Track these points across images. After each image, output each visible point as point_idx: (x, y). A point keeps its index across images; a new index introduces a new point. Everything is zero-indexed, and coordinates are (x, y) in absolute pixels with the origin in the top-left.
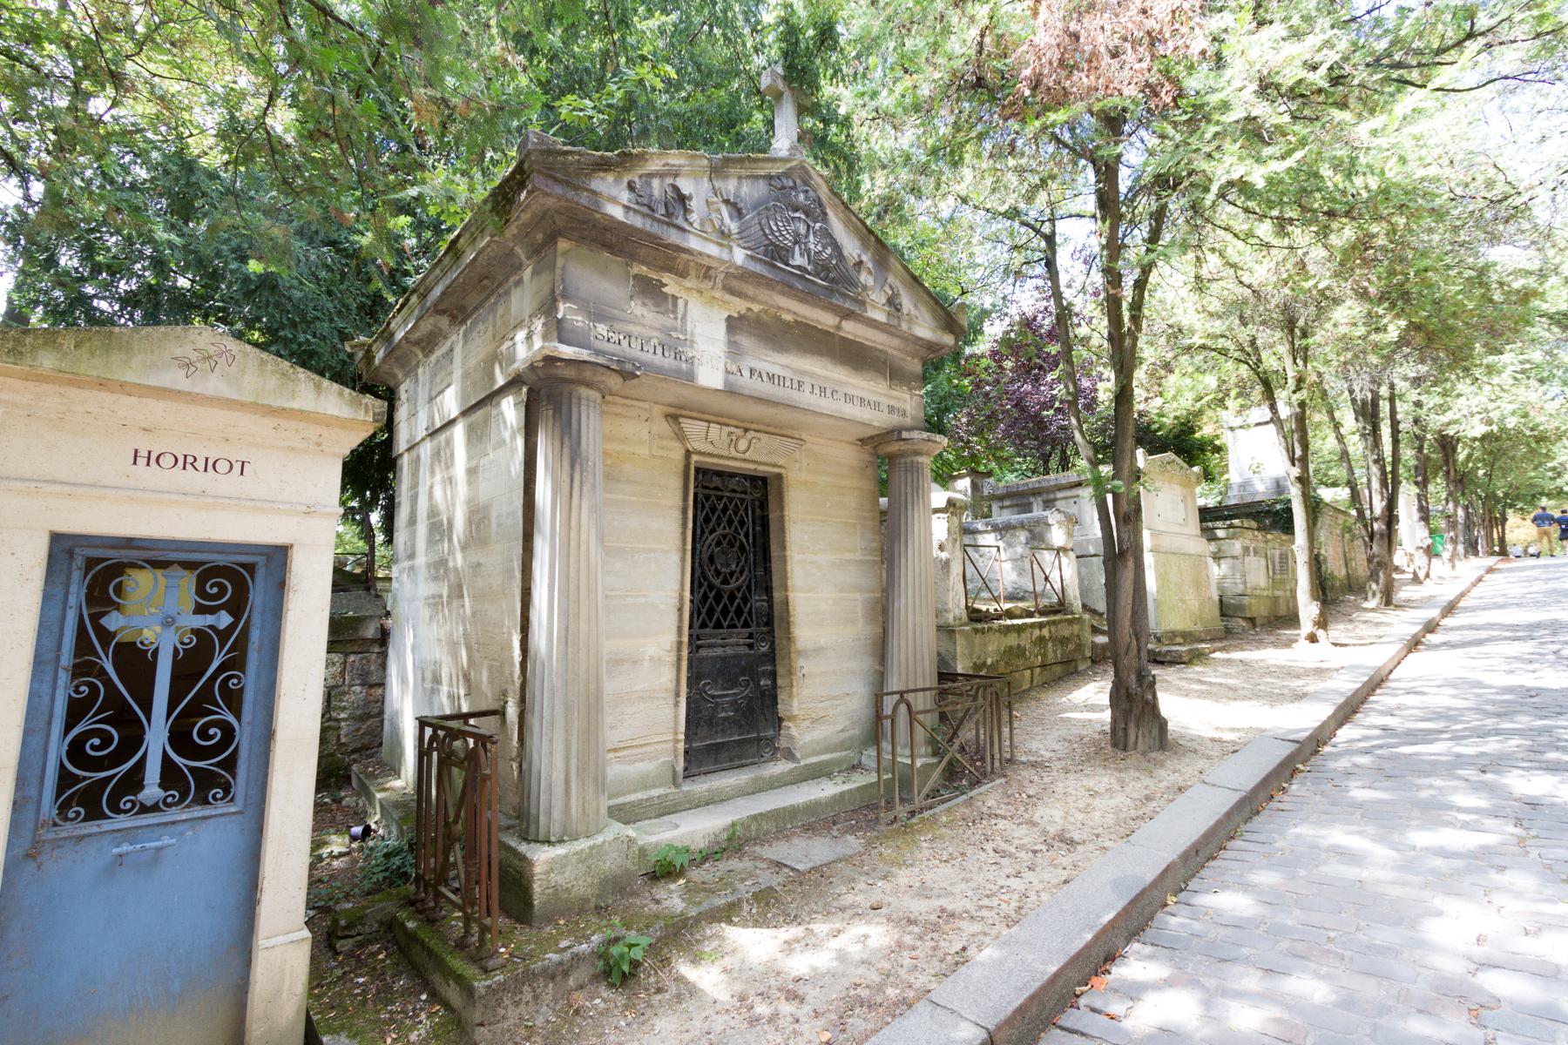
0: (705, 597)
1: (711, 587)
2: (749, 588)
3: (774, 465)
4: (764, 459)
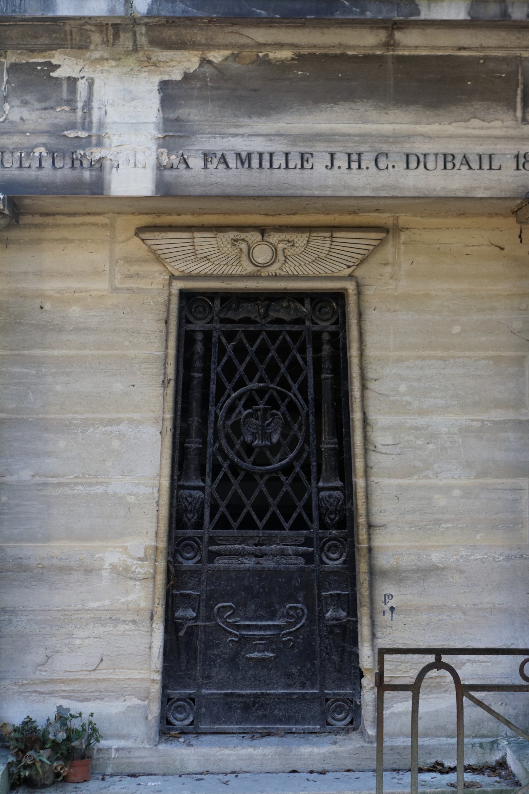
1: (234, 469)
2: (306, 468)
4: (310, 270)
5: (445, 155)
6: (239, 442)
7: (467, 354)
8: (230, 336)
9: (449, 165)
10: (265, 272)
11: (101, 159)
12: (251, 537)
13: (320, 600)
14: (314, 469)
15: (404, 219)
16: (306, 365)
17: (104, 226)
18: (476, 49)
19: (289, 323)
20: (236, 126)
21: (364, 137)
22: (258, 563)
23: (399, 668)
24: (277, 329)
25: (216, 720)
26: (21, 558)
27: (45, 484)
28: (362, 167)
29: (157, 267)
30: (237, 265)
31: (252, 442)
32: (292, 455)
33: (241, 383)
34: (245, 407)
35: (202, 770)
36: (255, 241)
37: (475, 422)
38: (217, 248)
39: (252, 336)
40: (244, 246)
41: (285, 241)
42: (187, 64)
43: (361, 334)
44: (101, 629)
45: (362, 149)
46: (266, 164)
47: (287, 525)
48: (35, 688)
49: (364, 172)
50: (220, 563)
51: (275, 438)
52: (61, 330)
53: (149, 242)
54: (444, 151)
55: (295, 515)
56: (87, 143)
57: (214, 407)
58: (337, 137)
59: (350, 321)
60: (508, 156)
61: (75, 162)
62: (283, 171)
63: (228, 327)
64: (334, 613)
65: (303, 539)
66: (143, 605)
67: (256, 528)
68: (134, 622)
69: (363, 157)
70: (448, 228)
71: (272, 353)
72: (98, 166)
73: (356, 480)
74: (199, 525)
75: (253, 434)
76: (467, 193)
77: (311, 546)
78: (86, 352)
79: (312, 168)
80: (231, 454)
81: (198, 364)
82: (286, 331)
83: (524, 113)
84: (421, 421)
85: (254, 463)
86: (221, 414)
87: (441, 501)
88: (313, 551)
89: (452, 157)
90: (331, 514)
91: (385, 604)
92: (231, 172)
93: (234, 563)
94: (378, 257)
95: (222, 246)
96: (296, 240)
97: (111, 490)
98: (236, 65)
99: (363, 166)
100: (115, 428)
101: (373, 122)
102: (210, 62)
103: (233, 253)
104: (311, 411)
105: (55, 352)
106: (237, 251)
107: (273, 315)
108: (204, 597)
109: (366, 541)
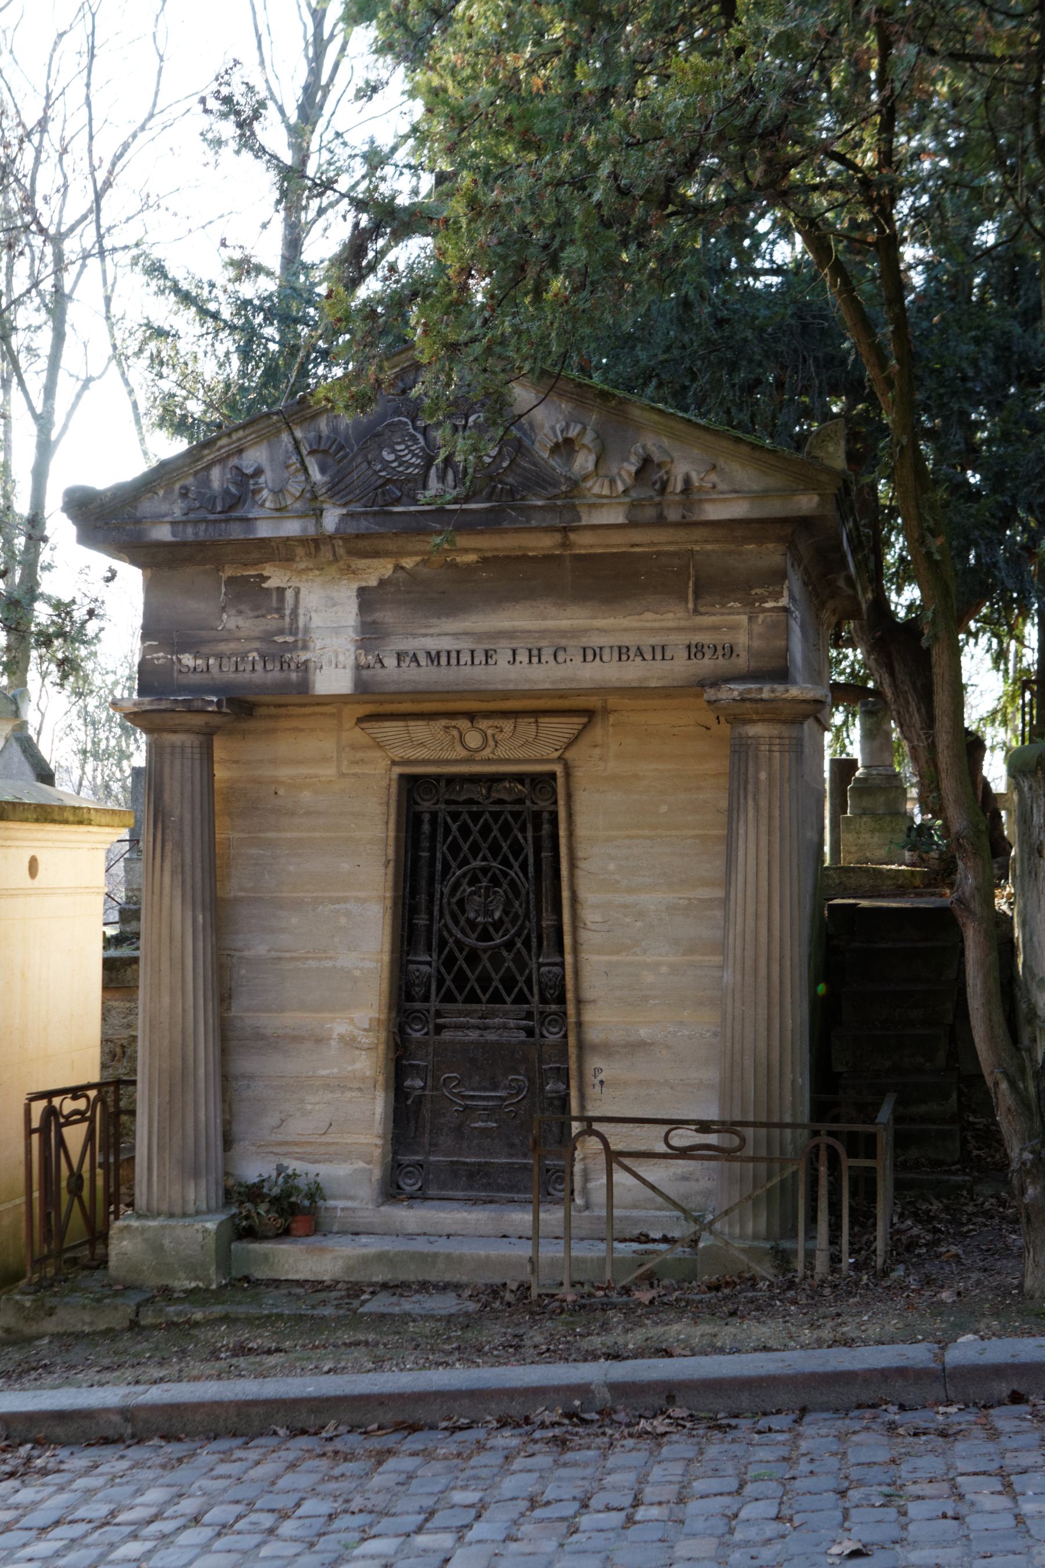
2: (527, 943)
5: (620, 648)
7: (674, 832)
8: (455, 816)
9: (624, 657)
10: (478, 756)
11: (306, 662)
12: (476, 1011)
13: (541, 1073)
15: (612, 702)
17: (332, 715)
18: (648, 545)
19: (511, 803)
20: (426, 627)
21: (543, 633)
25: (443, 1186)
27: (279, 959)
29: (379, 754)
33: (465, 862)
34: (470, 884)
35: (421, 1231)
39: (475, 816)
40: (455, 733)
42: (383, 571)
44: (330, 1096)
45: (542, 643)
46: (453, 661)
47: (508, 999)
48: (271, 1149)
49: (543, 666)
50: (446, 1035)
51: (497, 915)
52: (293, 814)
55: (516, 989)
56: (293, 647)
62: (469, 667)
63: (453, 808)
66: (368, 1073)
67: (479, 1001)
68: (360, 1089)
69: (543, 652)
71: (495, 832)
74: (426, 998)
78: (317, 835)
80: (456, 931)
81: (426, 844)
83: (695, 604)
84: (629, 899)
85: (478, 939)
86: (446, 891)
87: (649, 978)
92: (422, 670)
93: (459, 1035)
94: (586, 739)
97: (338, 965)
98: (426, 570)
99: (543, 660)
100: (342, 906)
101: (552, 619)
102: (402, 568)
105: (288, 835)
107: (495, 796)
108: (430, 1067)
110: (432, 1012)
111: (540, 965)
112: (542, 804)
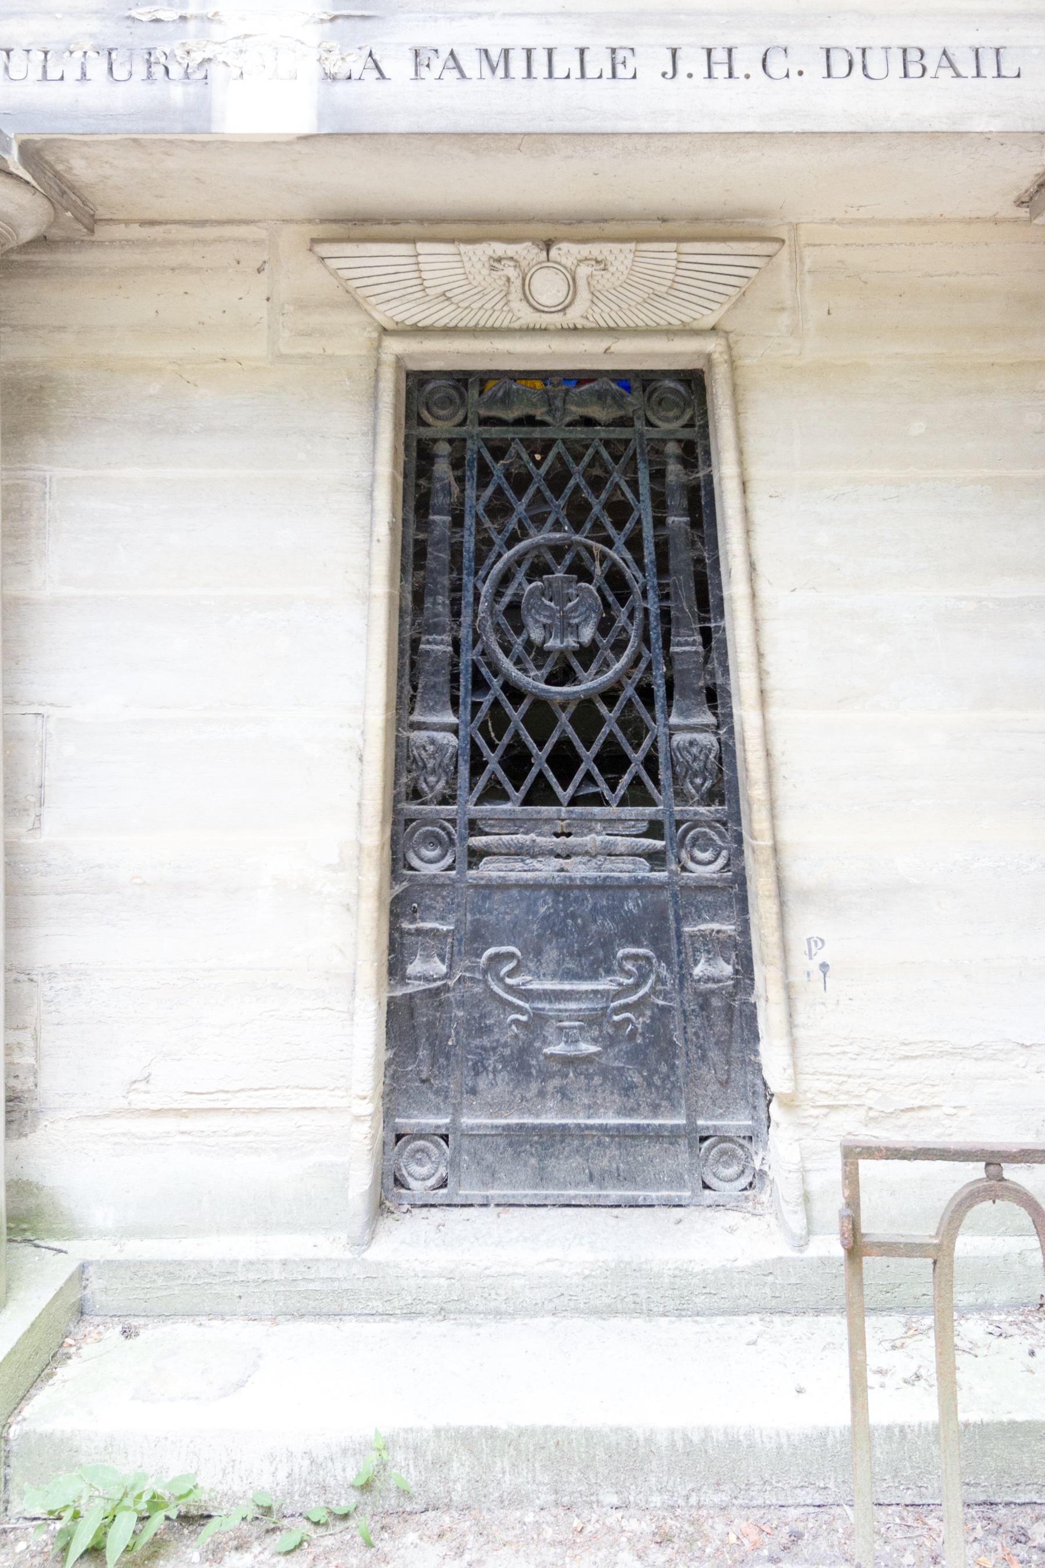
0: (499, 720)
1: (515, 694)
2: (646, 693)
3: (689, 331)
6: (519, 641)
9: (915, 70)
12: (548, 821)
14: (660, 692)
16: (639, 501)
22: (562, 870)
23: (844, 1088)
24: (583, 436)
26: (100, 866)
28: (736, 74)
29: (353, 318)
30: (502, 310)
31: (544, 642)
32: (617, 666)
36: (534, 262)
37: (964, 602)
38: (463, 277)
41: (591, 259)
43: (739, 437)
46: (540, 67)
50: (490, 870)
51: (587, 633)
53: (333, 264)
54: (904, 43)
57: (471, 578)
58: (682, 17)
59: (718, 411)
60: (1035, 51)
61: (154, 69)
63: (495, 432)
64: (710, 968)
65: (645, 824)
70: (892, 244)
72: (200, 74)
73: (744, 714)
75: (544, 626)
76: (954, 124)
77: (661, 837)
79: (634, 77)
80: (507, 664)
82: (601, 440)
86: (486, 589)
88: (665, 847)
89: (919, 54)
90: (696, 775)
91: (811, 958)
93: (516, 871)
95: (472, 270)
96: (611, 258)
103: (494, 285)
104: (650, 584)
106: (501, 282)
109: (768, 835)
110: (462, 822)
111: (673, 729)
112: (665, 426)
